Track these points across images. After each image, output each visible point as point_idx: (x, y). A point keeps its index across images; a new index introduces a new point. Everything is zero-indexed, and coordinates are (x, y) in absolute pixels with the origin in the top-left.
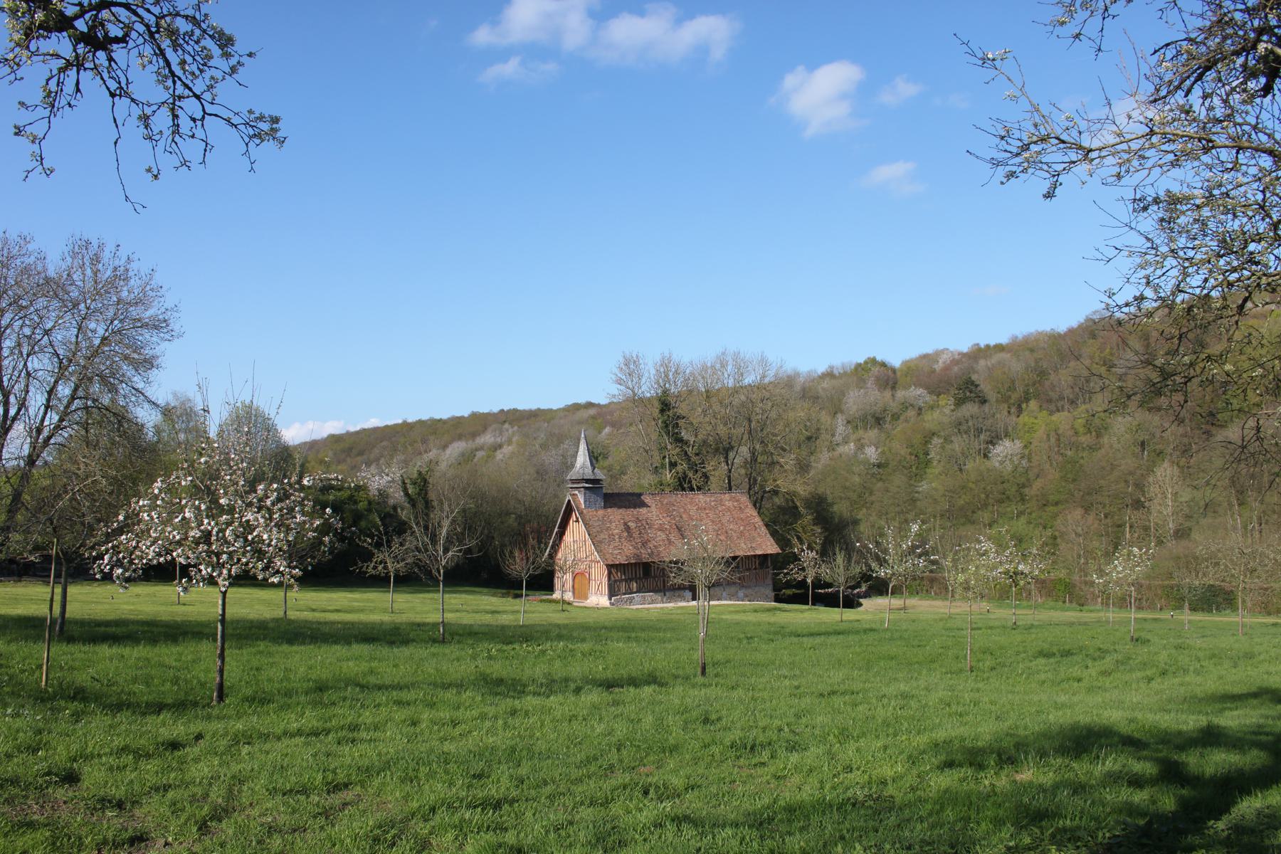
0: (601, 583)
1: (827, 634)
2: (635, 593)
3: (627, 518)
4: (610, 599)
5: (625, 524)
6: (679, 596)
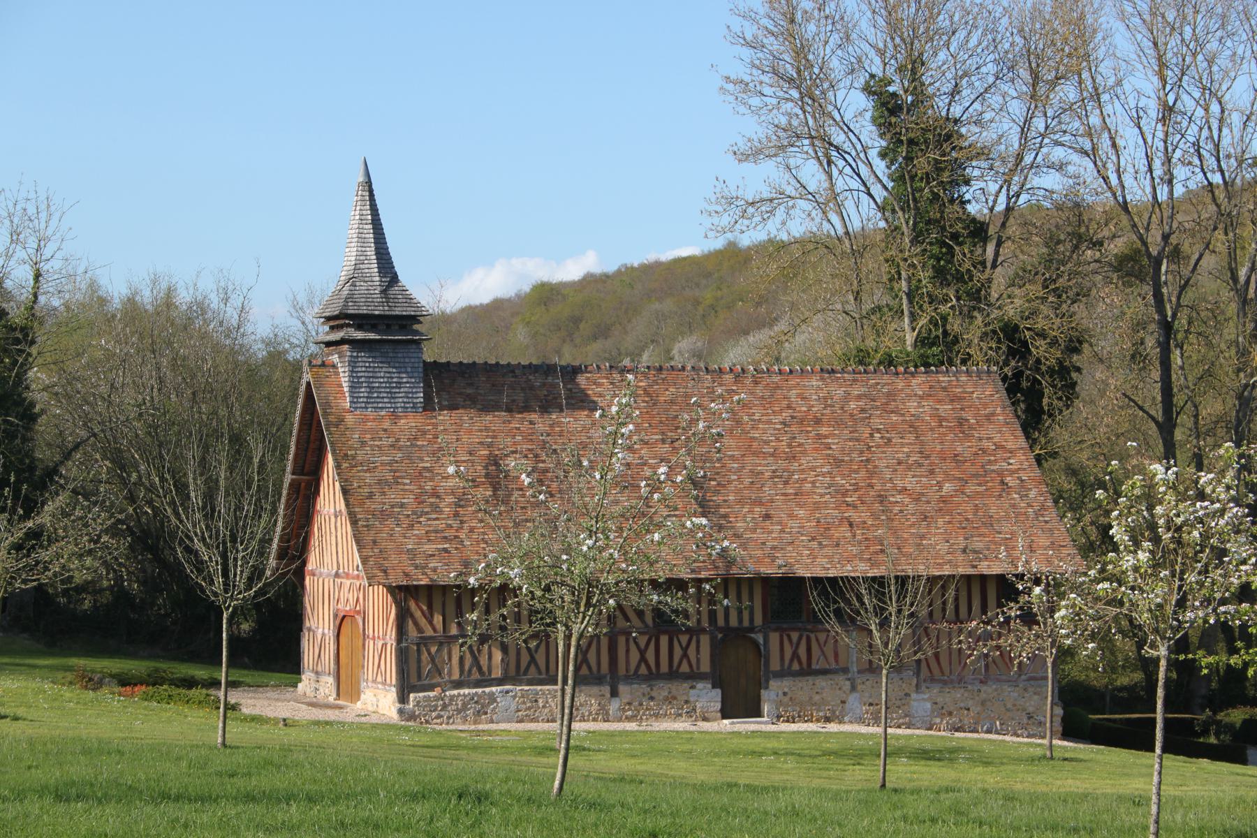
0: (385, 645)
1: (126, 794)
2: (500, 682)
3: (505, 442)
4: (403, 699)
5: (494, 461)
6: (670, 699)
